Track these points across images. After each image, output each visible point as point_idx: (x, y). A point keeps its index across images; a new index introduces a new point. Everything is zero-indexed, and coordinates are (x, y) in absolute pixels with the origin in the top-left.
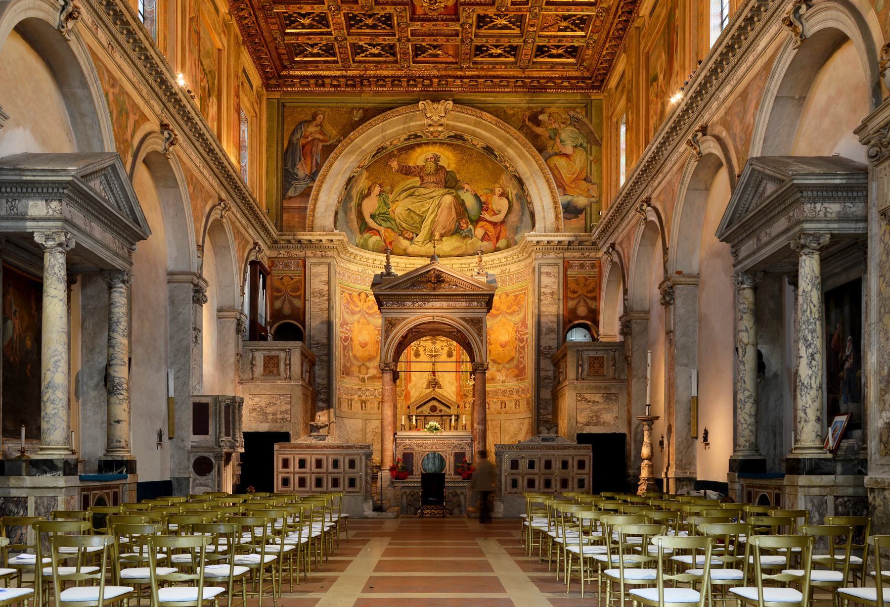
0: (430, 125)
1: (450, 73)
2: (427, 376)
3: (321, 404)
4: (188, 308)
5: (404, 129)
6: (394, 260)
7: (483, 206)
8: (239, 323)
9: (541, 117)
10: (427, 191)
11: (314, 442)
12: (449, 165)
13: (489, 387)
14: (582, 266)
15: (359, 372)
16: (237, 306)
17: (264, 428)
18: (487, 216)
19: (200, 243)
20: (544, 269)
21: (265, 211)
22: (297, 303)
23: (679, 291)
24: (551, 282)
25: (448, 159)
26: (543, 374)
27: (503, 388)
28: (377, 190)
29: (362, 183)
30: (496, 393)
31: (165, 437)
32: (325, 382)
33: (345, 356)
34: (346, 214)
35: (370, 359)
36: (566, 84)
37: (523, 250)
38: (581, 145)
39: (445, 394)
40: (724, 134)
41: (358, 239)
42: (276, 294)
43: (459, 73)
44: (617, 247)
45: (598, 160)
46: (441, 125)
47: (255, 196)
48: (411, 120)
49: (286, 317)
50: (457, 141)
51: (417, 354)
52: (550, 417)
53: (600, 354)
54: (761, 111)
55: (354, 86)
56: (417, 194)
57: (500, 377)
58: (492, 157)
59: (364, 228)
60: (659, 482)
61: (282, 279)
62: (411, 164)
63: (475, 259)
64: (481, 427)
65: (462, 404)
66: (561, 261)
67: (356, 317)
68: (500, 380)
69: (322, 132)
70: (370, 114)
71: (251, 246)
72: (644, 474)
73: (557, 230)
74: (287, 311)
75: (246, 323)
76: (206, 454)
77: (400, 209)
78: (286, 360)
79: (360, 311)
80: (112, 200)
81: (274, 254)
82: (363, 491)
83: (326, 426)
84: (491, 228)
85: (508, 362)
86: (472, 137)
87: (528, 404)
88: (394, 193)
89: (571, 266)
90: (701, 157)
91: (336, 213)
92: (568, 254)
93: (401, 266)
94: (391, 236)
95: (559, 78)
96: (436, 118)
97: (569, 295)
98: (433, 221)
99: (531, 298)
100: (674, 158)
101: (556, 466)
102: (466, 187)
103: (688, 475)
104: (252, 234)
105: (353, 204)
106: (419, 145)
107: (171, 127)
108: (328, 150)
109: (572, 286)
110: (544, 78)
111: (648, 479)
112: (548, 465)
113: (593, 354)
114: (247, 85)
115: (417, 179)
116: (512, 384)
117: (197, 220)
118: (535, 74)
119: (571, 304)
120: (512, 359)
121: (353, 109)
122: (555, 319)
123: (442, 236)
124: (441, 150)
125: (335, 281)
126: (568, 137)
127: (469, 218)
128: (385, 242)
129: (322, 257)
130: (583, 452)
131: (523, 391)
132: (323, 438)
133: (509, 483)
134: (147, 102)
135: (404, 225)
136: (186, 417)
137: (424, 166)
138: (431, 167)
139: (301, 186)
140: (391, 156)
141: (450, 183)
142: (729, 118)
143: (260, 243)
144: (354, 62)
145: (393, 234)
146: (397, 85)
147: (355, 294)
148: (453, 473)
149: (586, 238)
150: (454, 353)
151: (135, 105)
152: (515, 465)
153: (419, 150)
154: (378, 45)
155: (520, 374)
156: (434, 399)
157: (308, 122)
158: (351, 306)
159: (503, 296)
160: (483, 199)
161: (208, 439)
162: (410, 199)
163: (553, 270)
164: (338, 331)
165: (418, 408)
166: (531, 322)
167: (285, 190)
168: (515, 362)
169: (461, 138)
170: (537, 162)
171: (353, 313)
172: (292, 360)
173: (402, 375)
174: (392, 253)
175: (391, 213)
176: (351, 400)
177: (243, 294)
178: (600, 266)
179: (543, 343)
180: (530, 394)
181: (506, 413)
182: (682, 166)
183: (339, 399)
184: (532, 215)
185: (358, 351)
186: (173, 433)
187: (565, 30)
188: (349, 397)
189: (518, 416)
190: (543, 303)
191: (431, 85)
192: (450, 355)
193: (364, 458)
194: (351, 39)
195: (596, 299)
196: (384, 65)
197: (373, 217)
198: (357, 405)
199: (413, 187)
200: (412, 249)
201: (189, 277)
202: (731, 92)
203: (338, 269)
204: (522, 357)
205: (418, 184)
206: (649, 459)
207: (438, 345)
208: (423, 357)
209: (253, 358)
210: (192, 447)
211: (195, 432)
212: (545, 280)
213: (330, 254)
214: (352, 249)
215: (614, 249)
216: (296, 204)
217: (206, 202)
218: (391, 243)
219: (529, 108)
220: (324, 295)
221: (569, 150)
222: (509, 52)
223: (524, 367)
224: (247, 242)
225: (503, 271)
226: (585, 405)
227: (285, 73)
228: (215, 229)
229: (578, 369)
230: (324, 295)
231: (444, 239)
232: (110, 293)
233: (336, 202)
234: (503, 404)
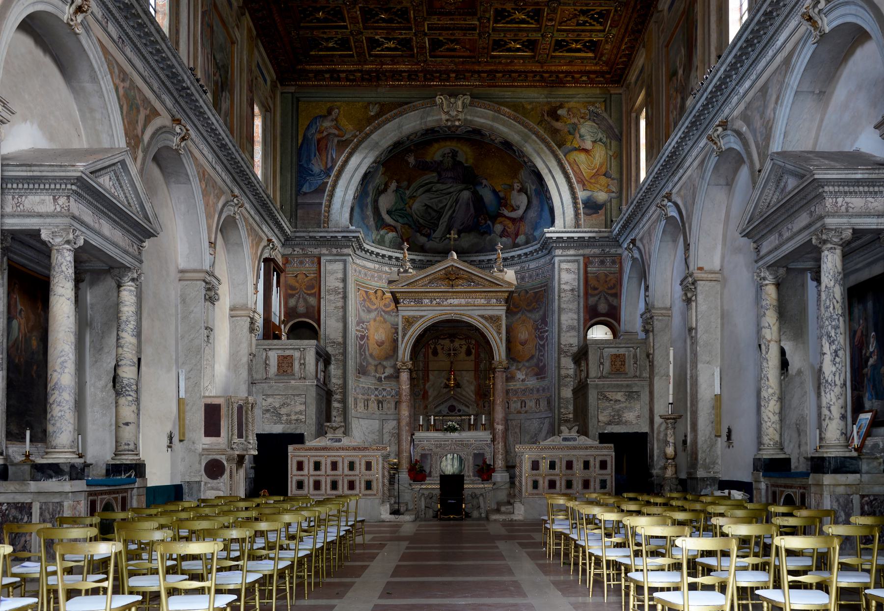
4: (199, 307)
8: (252, 322)
9: (559, 112)
10: (444, 187)
12: (467, 160)
14: (602, 262)
15: (376, 371)
16: (251, 304)
18: (506, 212)
19: (213, 240)
22: (312, 301)
27: (523, 388)
31: (176, 439)
32: (340, 382)
34: (362, 210)
38: (601, 140)
40: (744, 128)
42: (290, 292)
44: (638, 243)
47: (269, 192)
49: (300, 316)
51: (435, 353)
55: (369, 80)
56: (434, 189)
61: (296, 276)
62: (428, 159)
66: (581, 258)
67: (373, 315)
71: (264, 243)
74: (301, 309)
76: (218, 457)
79: (376, 309)
80: (122, 196)
81: (288, 251)
82: (380, 494)
85: (528, 361)
88: (411, 188)
89: (591, 263)
97: (590, 291)
98: (451, 217)
100: (694, 153)
101: (578, 466)
102: (484, 182)
106: (437, 140)
107: (183, 122)
109: (593, 283)
110: (562, 72)
112: (569, 465)
114: (260, 79)
117: (209, 216)
120: (532, 357)
121: (369, 103)
124: (459, 145)
126: (588, 132)
130: (605, 452)
131: (544, 390)
132: (340, 440)
133: (530, 484)
134: (158, 97)
135: (421, 221)
136: (198, 419)
137: (441, 161)
142: (749, 113)
143: (274, 239)
144: (370, 56)
147: (372, 292)
151: (146, 100)
153: (436, 146)
154: (394, 39)
157: (324, 117)
160: (502, 194)
161: (220, 442)
162: (428, 194)
167: (299, 186)
168: (535, 360)
172: (307, 359)
175: (408, 209)
178: (621, 263)
181: (526, 412)
182: (702, 162)
189: (537, 416)
192: (468, 353)
193: (380, 459)
194: (368, 33)
195: (617, 295)
197: (389, 212)
202: (751, 87)
204: (543, 356)
205: (435, 180)
207: (457, 344)
209: (267, 358)
210: (203, 449)
211: (207, 434)
213: (346, 251)
215: (634, 245)
221: (588, 145)
222: (527, 47)
223: (544, 366)
224: (261, 239)
228: (227, 227)
231: (462, 235)
232: (119, 292)
234: (523, 403)
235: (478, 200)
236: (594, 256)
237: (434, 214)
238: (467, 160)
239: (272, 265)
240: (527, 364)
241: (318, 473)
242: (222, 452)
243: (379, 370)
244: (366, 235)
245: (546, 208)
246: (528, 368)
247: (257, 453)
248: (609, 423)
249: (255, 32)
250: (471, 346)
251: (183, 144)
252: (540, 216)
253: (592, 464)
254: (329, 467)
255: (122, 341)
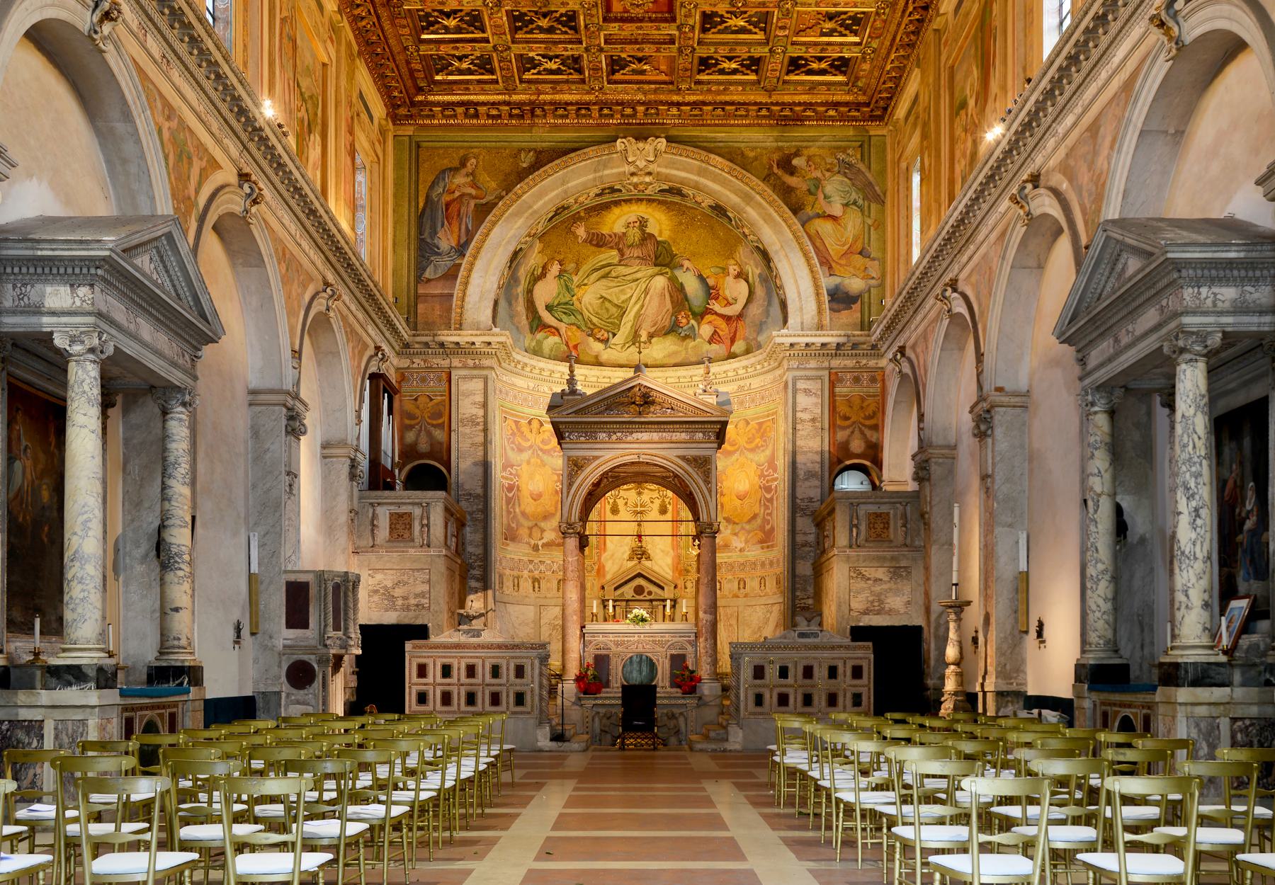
0: (633, 174)
1: (662, 97)
2: (630, 542)
3: (473, 584)
4: (277, 443)
5: (595, 179)
6: (580, 371)
7: (711, 292)
8: (354, 465)
9: (795, 162)
11: (463, 639)
12: (661, 233)
13: (721, 558)
14: (857, 380)
15: (530, 536)
16: (351, 440)
17: (390, 618)
18: (717, 307)
19: (297, 348)
20: (801, 385)
21: (391, 299)
22: (439, 435)
23: (1000, 416)
24: (811, 404)
25: (660, 223)
26: (799, 538)
27: (741, 560)
28: (555, 269)
29: (534, 260)
30: (731, 566)
31: (245, 632)
32: (479, 551)
33: (509, 512)
35: (546, 517)
36: (832, 113)
37: (770, 356)
38: (855, 203)
39: (656, 568)
41: (529, 340)
42: (407, 422)
43: (675, 98)
44: (909, 352)
45: (880, 225)
46: (650, 174)
48: (605, 167)
49: (422, 456)
50: (672, 197)
51: (615, 510)
52: (810, 601)
53: (884, 509)
54: (1119, 151)
55: (521, 117)
56: (613, 274)
57: (737, 543)
58: (725, 221)
59: (537, 325)
60: (971, 699)
61: (416, 399)
62: (605, 231)
63: (700, 370)
64: (709, 617)
65: (680, 583)
67: (525, 456)
68: (737, 548)
69: (474, 185)
70: (544, 158)
71: (371, 351)
72: (950, 685)
73: (820, 327)
74: (424, 446)
75: (364, 464)
76: (305, 658)
77: (589, 297)
78: (422, 519)
79: (531, 447)
80: (168, 283)
81: (405, 363)
82: (536, 712)
83: (482, 615)
84: (722, 324)
85: (749, 521)
86: (695, 191)
87: (778, 582)
89: (841, 380)
90: (1032, 221)
91: (496, 303)
92: (836, 363)
93: (591, 381)
94: (577, 336)
95: (822, 104)
96: (641, 164)
99: (783, 427)
100: (991, 221)
101: (820, 673)
102: (686, 264)
103: (1014, 687)
104: (372, 335)
105: (520, 289)
106: (617, 203)
107: (253, 178)
108: (484, 210)
109: (842, 409)
110: (800, 104)
111: (956, 694)
113: (873, 509)
114: (364, 116)
115: (615, 252)
116: (755, 553)
117: (291, 313)
118: (787, 99)
119: (841, 436)
120: (755, 516)
121: (520, 150)
122: (818, 458)
123: (651, 336)
124: (650, 210)
125: (494, 403)
126: (835, 190)
127: (690, 309)
128: (567, 345)
129: (475, 367)
130: (860, 653)
131: (771, 564)
132: (477, 634)
134: (218, 142)
135: (595, 320)
136: (277, 603)
137: (624, 234)
138: (634, 235)
139: (444, 264)
140: (576, 218)
141: (663, 258)
143: (385, 347)
144: (521, 81)
145: (579, 333)
146: (584, 116)
147: (524, 422)
148: (668, 684)
149: (862, 339)
150: (670, 508)
151: (201, 146)
152: (759, 672)
153: (616, 211)
154: (557, 56)
155: (766, 539)
156: (640, 575)
157: (455, 170)
158: (519, 439)
159: (741, 425)
160: (711, 282)
161: (309, 635)
162: (604, 282)
163: (814, 386)
164: (499, 476)
165: (616, 589)
166: (782, 463)
167: (420, 269)
168: (759, 521)
169: (679, 192)
170: (789, 227)
171: (521, 450)
172: (432, 519)
173: (593, 540)
174: (578, 361)
175: (576, 303)
176: (518, 578)
177: (359, 421)
178: (883, 380)
179: (799, 494)
180: (781, 568)
181: (746, 596)
183: (501, 576)
184: (784, 305)
185: (529, 506)
186: (257, 627)
187: (830, 34)
188: (516, 573)
189: (763, 601)
190: (799, 434)
191: (634, 116)
192: (663, 511)
193: (537, 662)
195: (877, 428)
196: (565, 87)
197: (549, 308)
198: (526, 585)
199: (609, 265)
200: (606, 355)
201: (281, 398)
202: (1075, 124)
203: (499, 385)
204: (770, 514)
205: (616, 261)
206: (957, 664)
207: (646, 496)
208: (624, 514)
209: (374, 516)
210: (285, 646)
211: (291, 624)
212: (803, 401)
214: (519, 356)
215: (903, 355)
216: (437, 289)
217: (305, 287)
218: (576, 347)
219: (779, 149)
220: (478, 424)
221: (837, 210)
222: (748, 67)
223: (772, 529)
224: (366, 346)
225: (741, 388)
226: (862, 584)
227: (420, 98)
228: (318, 326)
229: (851, 531)
230: (478, 424)
231: (654, 340)
232: (164, 421)
233: (496, 286)
234: (742, 583)
235: (678, 291)
236: (846, 370)
237: (613, 310)
238: (661, 233)
239: (382, 384)
240: (747, 527)
241: (447, 681)
242: (311, 650)
243: (534, 534)
244: (516, 341)
245: (776, 302)
246: (749, 532)
247: (360, 652)
248: (866, 612)
249: (356, 48)
250: (667, 501)
251: (254, 210)
252: (767, 313)
253: (840, 670)
254: (463, 672)
255: (170, 492)
